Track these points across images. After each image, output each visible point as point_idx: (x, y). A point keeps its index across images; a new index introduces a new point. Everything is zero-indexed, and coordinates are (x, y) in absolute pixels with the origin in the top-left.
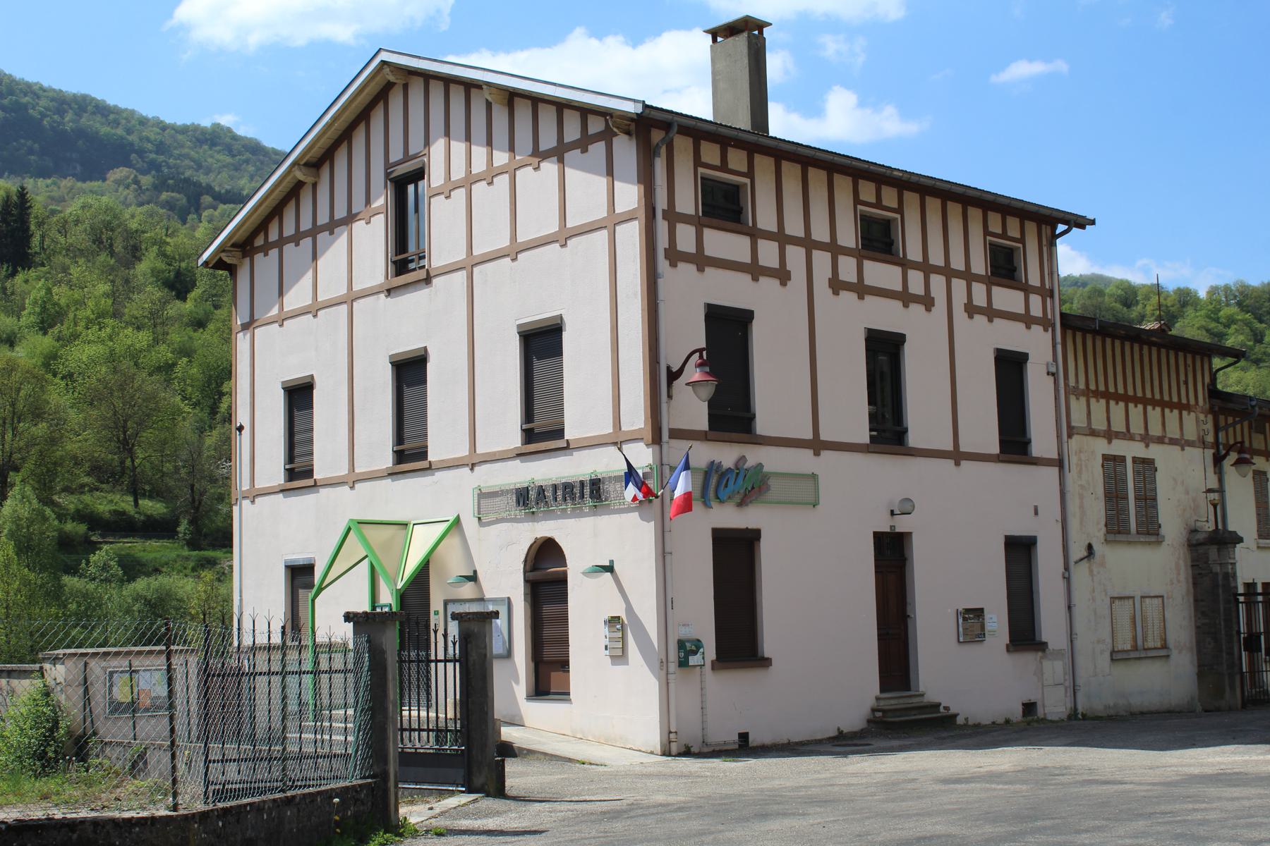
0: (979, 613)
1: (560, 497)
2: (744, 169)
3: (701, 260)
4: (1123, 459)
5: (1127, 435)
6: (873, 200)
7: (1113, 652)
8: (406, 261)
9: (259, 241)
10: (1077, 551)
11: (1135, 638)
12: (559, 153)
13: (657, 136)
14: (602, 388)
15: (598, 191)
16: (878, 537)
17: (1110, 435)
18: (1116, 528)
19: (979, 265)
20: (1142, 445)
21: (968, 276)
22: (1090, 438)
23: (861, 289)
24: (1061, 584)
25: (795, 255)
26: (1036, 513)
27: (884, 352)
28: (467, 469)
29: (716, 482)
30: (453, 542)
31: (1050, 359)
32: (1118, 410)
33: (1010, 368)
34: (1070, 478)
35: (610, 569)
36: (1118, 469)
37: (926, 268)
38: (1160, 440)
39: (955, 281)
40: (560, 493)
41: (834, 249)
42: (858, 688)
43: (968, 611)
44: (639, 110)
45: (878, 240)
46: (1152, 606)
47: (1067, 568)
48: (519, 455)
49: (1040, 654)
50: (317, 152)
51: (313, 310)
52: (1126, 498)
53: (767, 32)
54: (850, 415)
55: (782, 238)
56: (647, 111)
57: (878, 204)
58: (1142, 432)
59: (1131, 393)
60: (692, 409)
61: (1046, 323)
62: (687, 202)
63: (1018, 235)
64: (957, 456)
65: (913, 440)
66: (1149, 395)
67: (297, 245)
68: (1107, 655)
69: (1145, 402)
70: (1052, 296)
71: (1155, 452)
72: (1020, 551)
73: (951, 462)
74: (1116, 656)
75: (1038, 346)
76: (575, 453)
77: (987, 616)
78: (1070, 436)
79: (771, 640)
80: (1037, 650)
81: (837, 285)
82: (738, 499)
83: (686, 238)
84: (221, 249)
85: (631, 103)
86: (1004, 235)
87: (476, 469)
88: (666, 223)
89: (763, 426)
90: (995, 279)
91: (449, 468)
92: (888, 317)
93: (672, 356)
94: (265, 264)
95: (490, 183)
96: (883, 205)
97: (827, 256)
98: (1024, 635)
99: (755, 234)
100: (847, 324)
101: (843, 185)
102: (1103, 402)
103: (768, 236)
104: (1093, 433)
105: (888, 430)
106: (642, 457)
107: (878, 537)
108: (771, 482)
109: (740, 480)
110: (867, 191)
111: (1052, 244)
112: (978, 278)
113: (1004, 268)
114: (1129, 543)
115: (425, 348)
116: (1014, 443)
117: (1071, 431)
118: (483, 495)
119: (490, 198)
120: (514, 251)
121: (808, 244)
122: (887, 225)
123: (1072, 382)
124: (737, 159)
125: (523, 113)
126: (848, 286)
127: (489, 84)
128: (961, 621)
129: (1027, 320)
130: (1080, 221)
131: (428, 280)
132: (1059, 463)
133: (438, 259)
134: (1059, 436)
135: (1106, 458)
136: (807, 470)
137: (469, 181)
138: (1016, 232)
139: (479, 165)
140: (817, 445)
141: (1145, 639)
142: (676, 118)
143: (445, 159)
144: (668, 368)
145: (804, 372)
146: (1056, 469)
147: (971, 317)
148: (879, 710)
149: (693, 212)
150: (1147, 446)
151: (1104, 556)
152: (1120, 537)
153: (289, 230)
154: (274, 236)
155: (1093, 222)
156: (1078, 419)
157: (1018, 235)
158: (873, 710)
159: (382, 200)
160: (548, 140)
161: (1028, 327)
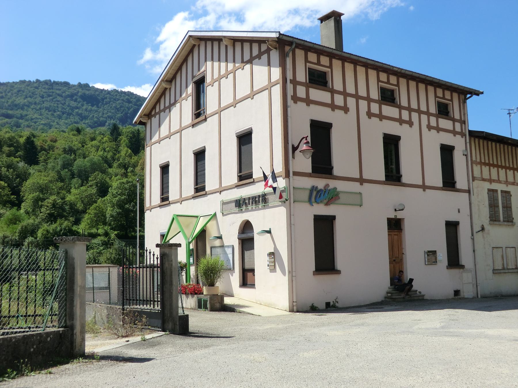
0: (434, 253)
1: (250, 203)
2: (328, 65)
3: (308, 101)
4: (496, 191)
5: (499, 181)
6: (442, 96)
7: (494, 270)
8: (199, 112)
9: (153, 113)
10: (477, 228)
11: (503, 264)
12: (250, 61)
13: (287, 48)
14: (267, 155)
15: (266, 74)
16: (389, 220)
17: (491, 181)
18: (494, 218)
19: (433, 109)
20: (505, 185)
21: (428, 114)
22: (482, 182)
23: (381, 117)
24: (470, 241)
25: (351, 102)
26: (459, 212)
27: (391, 144)
28: (218, 194)
29: (316, 195)
30: (213, 223)
31: (464, 149)
32: (494, 171)
33: (447, 152)
34: (473, 198)
35: (269, 232)
36: (495, 194)
37: (410, 109)
38: (513, 184)
39: (422, 116)
40: (251, 201)
41: (369, 99)
42: (381, 283)
43: (429, 252)
44: (278, 36)
45: (388, 97)
46: (510, 252)
47: (472, 235)
48: (236, 186)
49: (461, 270)
50: (170, 76)
51: (169, 137)
52: (498, 207)
53: (342, 17)
54: (376, 168)
55: (345, 94)
56: (281, 36)
57: (388, 82)
58: (505, 180)
59: (500, 164)
60: (304, 162)
61: (462, 134)
62: (302, 76)
63: (449, 98)
64: (424, 187)
65: (404, 180)
66: (500, 164)
67: (165, 112)
68: (491, 271)
69: (506, 168)
70: (465, 124)
71: (510, 188)
72: (452, 227)
73: (422, 190)
74: (495, 272)
75: (459, 144)
76: (257, 184)
77: (438, 254)
78: (473, 180)
79: (340, 263)
80: (460, 268)
81: (370, 115)
82: (325, 201)
83: (301, 91)
84: (140, 116)
85: (274, 33)
86: (444, 98)
87: (222, 193)
88: (292, 85)
89: (336, 172)
90: (440, 115)
91: (212, 193)
92: (393, 129)
93: (294, 140)
94: (155, 120)
95: (252, 99)
96: (392, 84)
97: (360, 94)
98: (454, 261)
99: (333, 92)
100: (375, 132)
101: (372, 73)
102: (488, 167)
103: (339, 93)
104: (484, 180)
105: (393, 175)
106: (281, 183)
107: (389, 220)
108: (340, 195)
109: (326, 195)
110: (383, 76)
111: (465, 102)
112: (432, 115)
113: (443, 111)
114: (500, 225)
115: (205, 147)
116: (449, 182)
117: (474, 179)
118: (224, 203)
119: (227, 83)
120: (234, 105)
121: (357, 97)
122: (392, 92)
123: (474, 159)
124: (325, 60)
125: (238, 46)
126: (375, 115)
127: (225, 37)
128: (426, 256)
129: (454, 132)
130: (476, 92)
131: (205, 120)
132: (469, 191)
133: (209, 111)
134: (468, 181)
135: (489, 190)
136: (358, 191)
137: (220, 78)
138: (449, 98)
139: (223, 72)
140: (361, 181)
141: (507, 265)
142: (295, 40)
143: (211, 69)
144: (293, 146)
145: (355, 150)
146: (468, 194)
147: (429, 130)
148: (389, 293)
149: (305, 81)
150: (507, 186)
151: (489, 230)
152: (495, 223)
153: (162, 107)
154: (157, 110)
155: (482, 93)
156: (477, 173)
157: (449, 98)
158: (387, 293)
159: (190, 89)
160: (247, 57)
161: (455, 136)
